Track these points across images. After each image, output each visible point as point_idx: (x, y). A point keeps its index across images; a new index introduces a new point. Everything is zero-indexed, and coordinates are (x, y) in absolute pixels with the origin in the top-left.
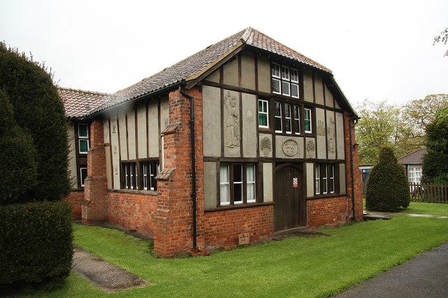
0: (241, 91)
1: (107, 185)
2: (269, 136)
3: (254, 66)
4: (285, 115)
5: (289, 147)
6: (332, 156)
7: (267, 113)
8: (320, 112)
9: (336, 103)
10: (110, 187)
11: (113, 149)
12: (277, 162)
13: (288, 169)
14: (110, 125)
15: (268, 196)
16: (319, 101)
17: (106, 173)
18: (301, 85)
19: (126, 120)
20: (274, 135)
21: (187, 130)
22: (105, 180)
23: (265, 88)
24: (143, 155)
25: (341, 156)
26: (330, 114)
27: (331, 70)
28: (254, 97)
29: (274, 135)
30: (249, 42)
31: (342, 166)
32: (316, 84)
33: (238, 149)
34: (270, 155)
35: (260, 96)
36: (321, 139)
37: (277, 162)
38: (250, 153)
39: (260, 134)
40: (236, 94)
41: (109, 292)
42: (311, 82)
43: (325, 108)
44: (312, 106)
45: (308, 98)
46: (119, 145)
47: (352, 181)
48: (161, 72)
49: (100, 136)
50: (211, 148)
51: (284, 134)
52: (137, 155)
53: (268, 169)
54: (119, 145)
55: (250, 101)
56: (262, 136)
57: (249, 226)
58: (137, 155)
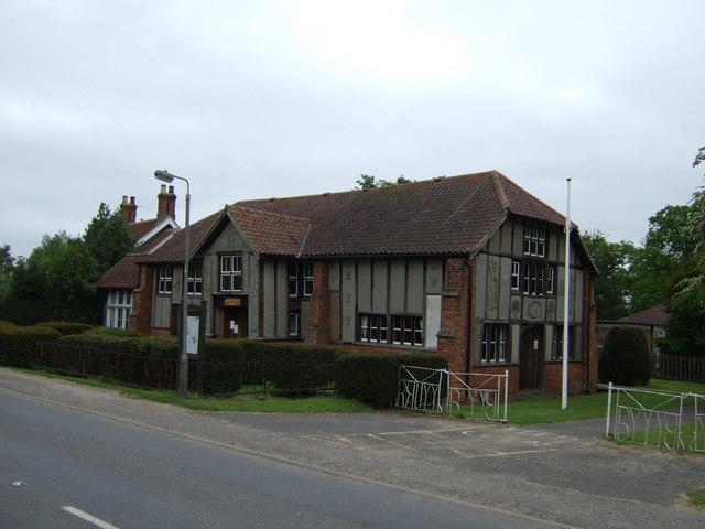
0: (500, 256)
2: (518, 298)
5: (534, 310)
10: (335, 336)
12: (523, 324)
13: (533, 331)
14: (341, 273)
18: (547, 243)
19: (372, 274)
20: (523, 296)
21: (466, 295)
22: (329, 330)
23: (518, 252)
24: (397, 308)
27: (627, 240)
29: (523, 296)
30: (514, 212)
33: (495, 311)
34: (519, 317)
35: (515, 260)
37: (523, 324)
38: (504, 317)
40: (497, 258)
41: (552, 524)
47: (589, 346)
49: (326, 281)
50: (479, 312)
51: (530, 296)
52: (388, 308)
53: (516, 330)
55: (507, 262)
56: (514, 298)
58: (388, 308)
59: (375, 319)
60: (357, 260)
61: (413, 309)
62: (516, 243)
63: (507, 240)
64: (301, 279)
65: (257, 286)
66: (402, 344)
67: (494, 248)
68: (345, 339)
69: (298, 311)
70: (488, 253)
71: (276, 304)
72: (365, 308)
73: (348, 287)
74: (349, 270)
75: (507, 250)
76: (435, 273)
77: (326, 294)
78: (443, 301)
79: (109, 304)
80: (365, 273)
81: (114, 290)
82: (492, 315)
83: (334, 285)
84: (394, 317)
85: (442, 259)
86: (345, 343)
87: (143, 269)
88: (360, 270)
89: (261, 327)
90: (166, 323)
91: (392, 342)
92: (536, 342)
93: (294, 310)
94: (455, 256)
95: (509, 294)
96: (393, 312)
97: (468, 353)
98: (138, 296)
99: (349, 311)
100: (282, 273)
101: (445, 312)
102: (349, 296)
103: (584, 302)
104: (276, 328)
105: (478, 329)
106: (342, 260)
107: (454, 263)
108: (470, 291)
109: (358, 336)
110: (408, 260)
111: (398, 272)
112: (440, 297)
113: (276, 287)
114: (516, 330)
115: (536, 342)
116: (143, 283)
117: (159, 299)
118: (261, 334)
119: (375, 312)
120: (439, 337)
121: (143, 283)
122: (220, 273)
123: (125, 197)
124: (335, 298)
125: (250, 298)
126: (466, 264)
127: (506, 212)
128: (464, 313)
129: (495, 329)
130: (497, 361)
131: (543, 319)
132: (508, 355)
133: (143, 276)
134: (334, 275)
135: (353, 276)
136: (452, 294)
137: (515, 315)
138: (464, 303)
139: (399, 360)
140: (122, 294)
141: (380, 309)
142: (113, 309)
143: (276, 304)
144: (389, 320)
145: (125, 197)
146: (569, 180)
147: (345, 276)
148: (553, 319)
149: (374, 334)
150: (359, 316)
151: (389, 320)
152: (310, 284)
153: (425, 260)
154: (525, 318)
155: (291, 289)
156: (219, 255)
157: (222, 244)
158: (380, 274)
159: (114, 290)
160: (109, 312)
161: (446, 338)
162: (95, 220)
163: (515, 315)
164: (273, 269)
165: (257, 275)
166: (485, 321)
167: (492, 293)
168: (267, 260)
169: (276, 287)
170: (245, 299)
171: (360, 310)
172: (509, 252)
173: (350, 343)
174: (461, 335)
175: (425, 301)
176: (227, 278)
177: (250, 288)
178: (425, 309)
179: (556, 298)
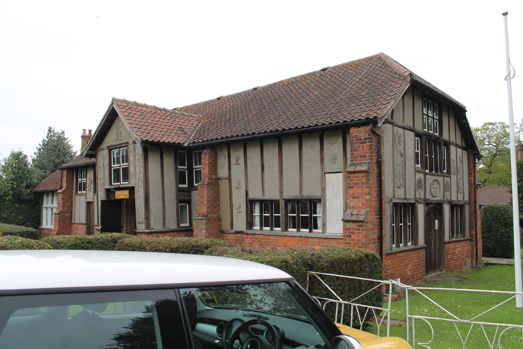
0: (404, 128)
1: (221, 226)
2: (421, 176)
3: (412, 101)
4: (432, 154)
5: (435, 189)
6: (460, 198)
7: (419, 151)
8: (453, 148)
9: (457, 125)
10: (226, 225)
11: (234, 185)
12: (427, 203)
15: (421, 241)
16: (453, 139)
17: (219, 210)
22: (219, 219)
23: (419, 128)
24: (292, 191)
25: (467, 198)
26: (459, 150)
28: (412, 134)
31: (467, 207)
32: (450, 120)
34: (422, 197)
35: (417, 135)
36: (453, 177)
37: (427, 203)
38: (411, 197)
39: (417, 174)
40: (401, 130)
42: (447, 118)
43: (457, 146)
44: (447, 144)
45: (445, 137)
46: (247, 179)
48: (318, 72)
49: (214, 167)
50: (388, 192)
52: (281, 193)
53: (421, 210)
54: (247, 179)
57: (410, 270)
58: (281, 193)
59: (268, 205)
60: (245, 142)
61: (310, 191)
62: (424, 118)
63: (409, 111)
64: (190, 169)
65: (142, 176)
66: (272, 229)
67: (398, 119)
68: (236, 228)
69: (189, 202)
70: (392, 124)
71: (163, 194)
72: (256, 194)
73: (238, 172)
74: (237, 154)
75: (409, 123)
76: (334, 148)
77: (215, 182)
78: (346, 179)
79: (45, 205)
80: (254, 154)
81: (48, 193)
82: (400, 194)
83: (223, 172)
84: (287, 201)
85: (342, 130)
86: (237, 232)
87: (65, 173)
88: (250, 153)
89: (147, 218)
90: (83, 220)
91: (286, 230)
92: (437, 221)
93: (184, 200)
94: (359, 124)
95: (413, 171)
96: (286, 196)
97: (380, 239)
98: (60, 196)
99: (239, 201)
100: (169, 162)
101: (351, 191)
102: (239, 183)
103: (470, 182)
104: (164, 219)
105: (388, 209)
106: (228, 144)
107: (361, 133)
108: (379, 164)
109: (250, 224)
110: (300, 135)
111: (291, 151)
112: (341, 175)
113: (162, 176)
114: (421, 210)
115: (437, 221)
116: (65, 185)
117: (78, 198)
118: (148, 226)
119: (267, 197)
120: (345, 221)
121: (65, 185)
122: (110, 167)
123: (84, 130)
124: (224, 185)
125: (136, 189)
126: (374, 133)
127: (409, 79)
128: (374, 191)
129: (404, 210)
130: (406, 245)
131: (442, 198)
132: (415, 240)
133: (65, 179)
134: (222, 161)
135: (242, 161)
136: (359, 168)
137: (420, 194)
138: (374, 180)
139: (305, 264)
140: (53, 196)
141: (272, 194)
142: (47, 208)
143: (163, 194)
144: (282, 205)
145: (84, 130)
146: (505, 14)
147: (233, 161)
148: (449, 198)
149: (265, 222)
150: (250, 203)
151: (282, 205)
152: (198, 172)
153: (321, 133)
154: (427, 197)
155: (180, 178)
156: (110, 149)
157: (111, 139)
158: (271, 153)
159: (48, 193)
160: (44, 211)
161: (354, 221)
162: (55, 146)
163: (420, 194)
164: (159, 158)
165: (142, 164)
166: (394, 201)
167: (399, 169)
168: (149, 147)
169: (162, 176)
170: (132, 190)
171: (251, 196)
172: (412, 126)
173: (241, 232)
174: (373, 218)
175: (323, 181)
176: (117, 171)
177: (136, 179)
178: (324, 190)
179: (450, 177)
